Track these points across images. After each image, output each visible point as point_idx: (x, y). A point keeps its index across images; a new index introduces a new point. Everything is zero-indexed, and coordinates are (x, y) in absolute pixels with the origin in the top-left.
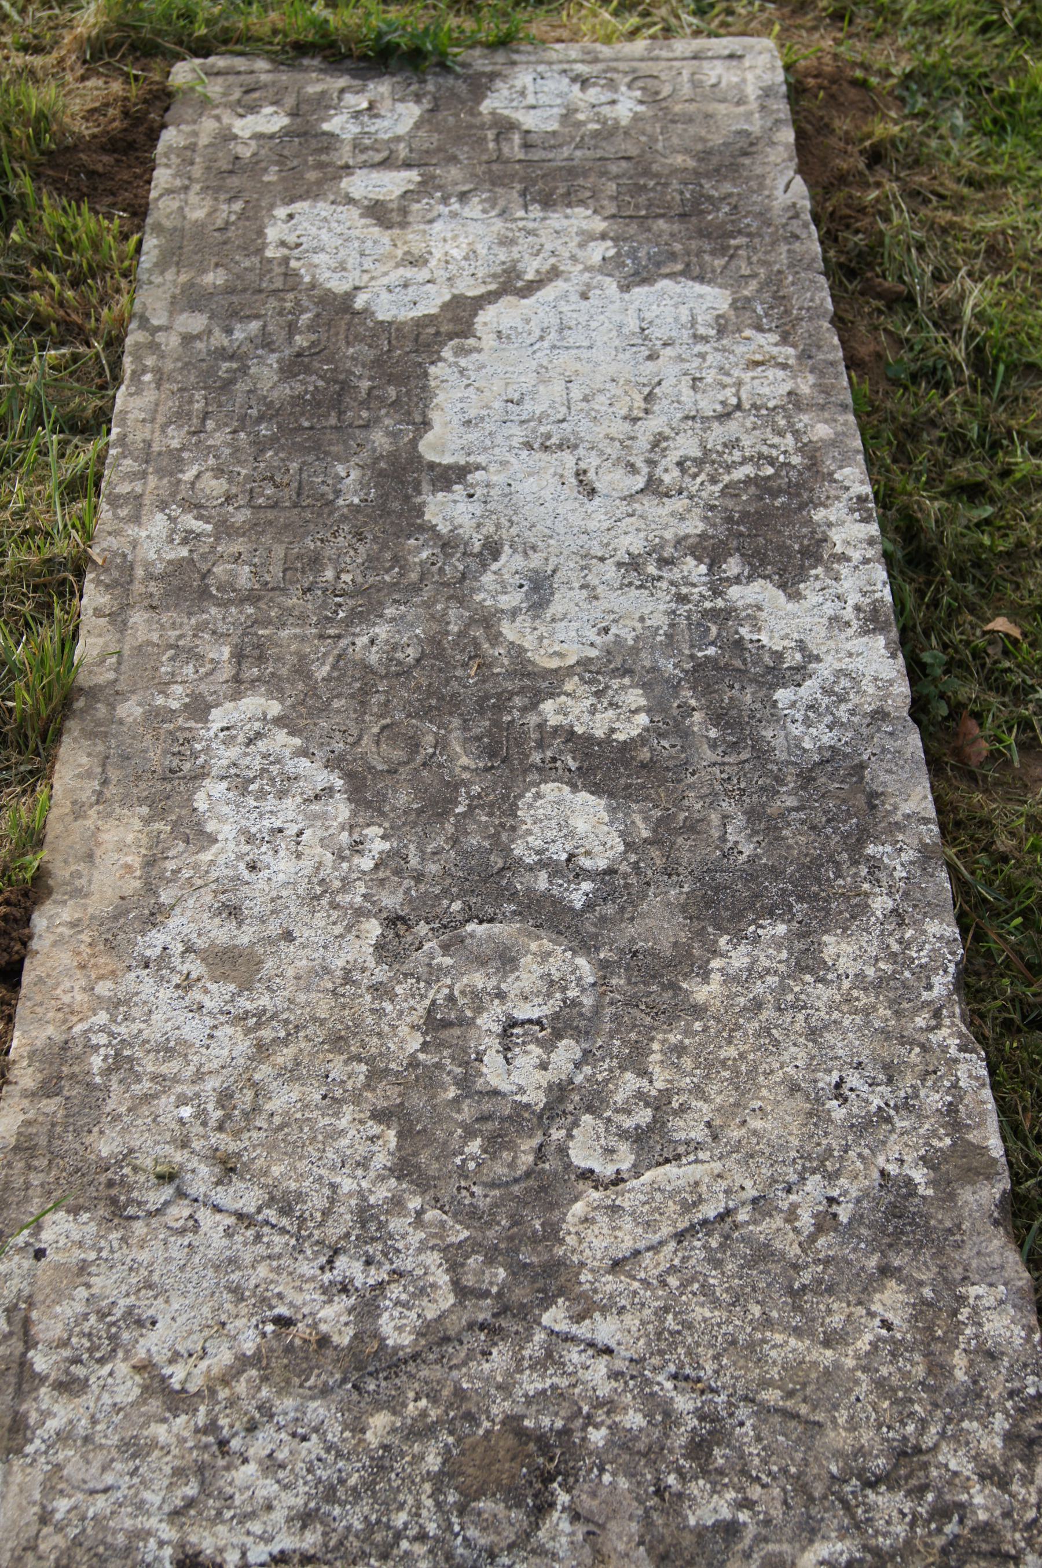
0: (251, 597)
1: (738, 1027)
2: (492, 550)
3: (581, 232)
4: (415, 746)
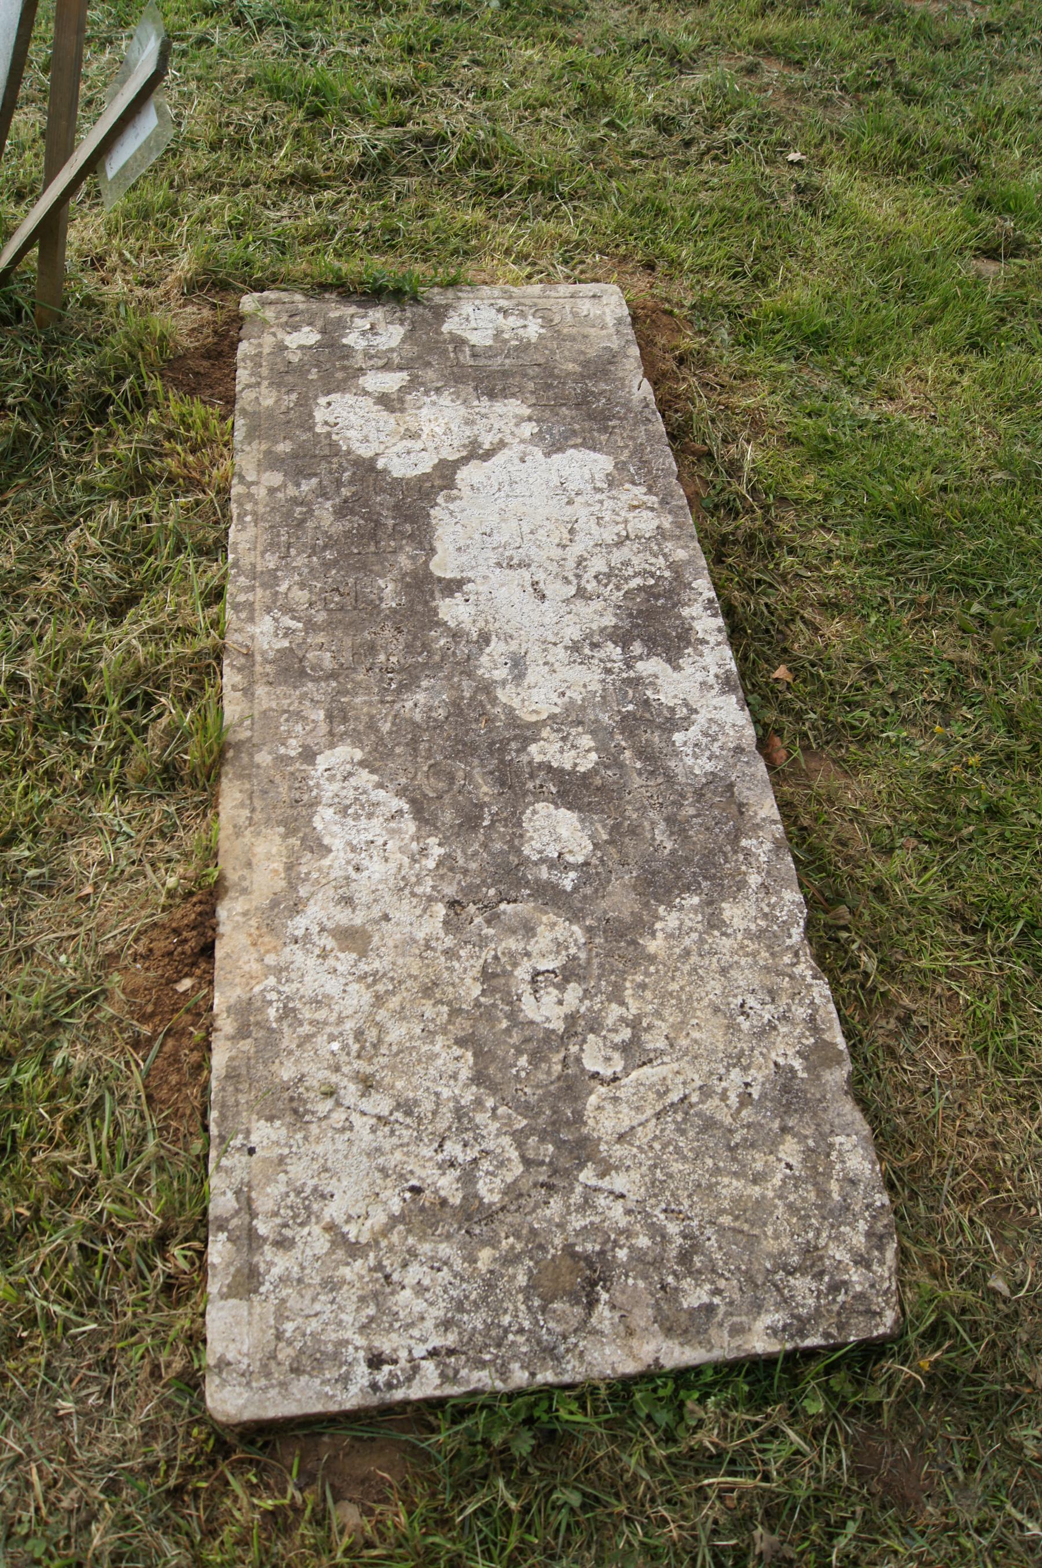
0: (333, 675)
1: (677, 969)
2: (485, 638)
3: (516, 416)
4: (452, 779)
